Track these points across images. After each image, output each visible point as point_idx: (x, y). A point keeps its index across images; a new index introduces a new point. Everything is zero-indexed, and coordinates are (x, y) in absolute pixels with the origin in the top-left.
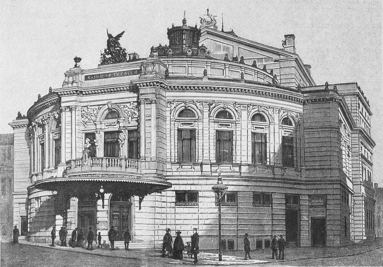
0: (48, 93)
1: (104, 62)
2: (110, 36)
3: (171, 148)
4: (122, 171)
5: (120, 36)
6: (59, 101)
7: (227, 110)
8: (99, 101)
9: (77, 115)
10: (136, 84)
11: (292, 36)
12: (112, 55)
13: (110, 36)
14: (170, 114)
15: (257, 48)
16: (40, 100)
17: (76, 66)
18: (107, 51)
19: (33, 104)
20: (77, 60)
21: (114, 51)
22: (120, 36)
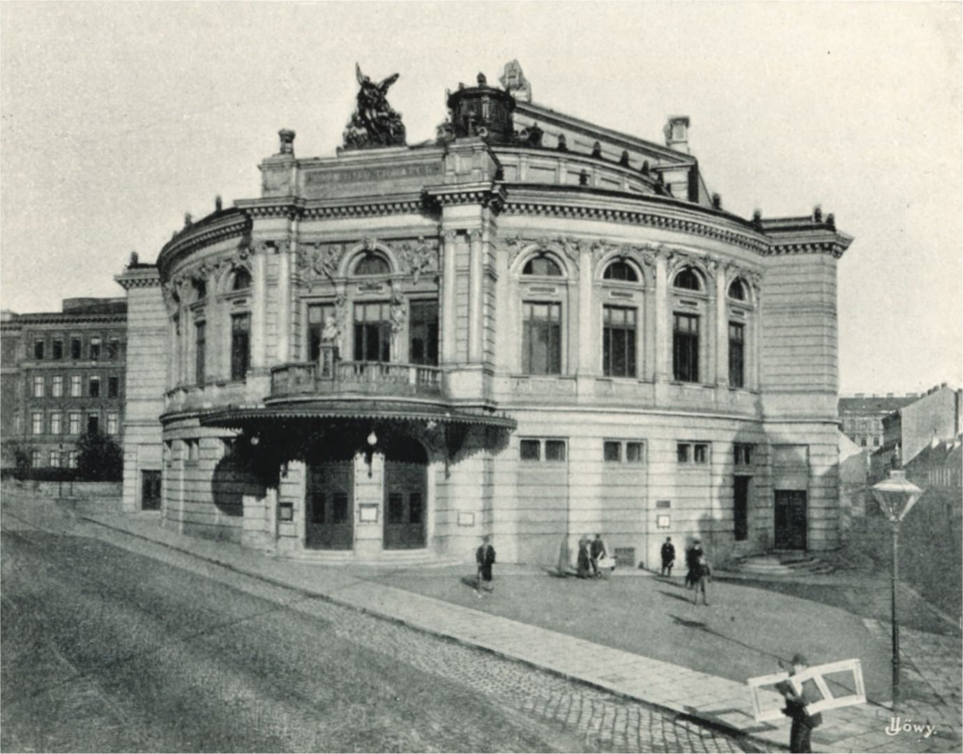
0: (212, 209)
1: (351, 142)
2: (366, 84)
3: (509, 348)
4: (389, 389)
5: (390, 81)
6: (247, 228)
7: (629, 262)
8: (568, 312)
9: (284, 265)
10: (435, 197)
11: (685, 121)
12: (369, 128)
13: (366, 84)
14: (510, 267)
15: (214, 238)
16: (191, 227)
17: (283, 151)
18: (359, 118)
19: (169, 239)
20: (287, 137)
21: (375, 119)
22: (390, 81)
